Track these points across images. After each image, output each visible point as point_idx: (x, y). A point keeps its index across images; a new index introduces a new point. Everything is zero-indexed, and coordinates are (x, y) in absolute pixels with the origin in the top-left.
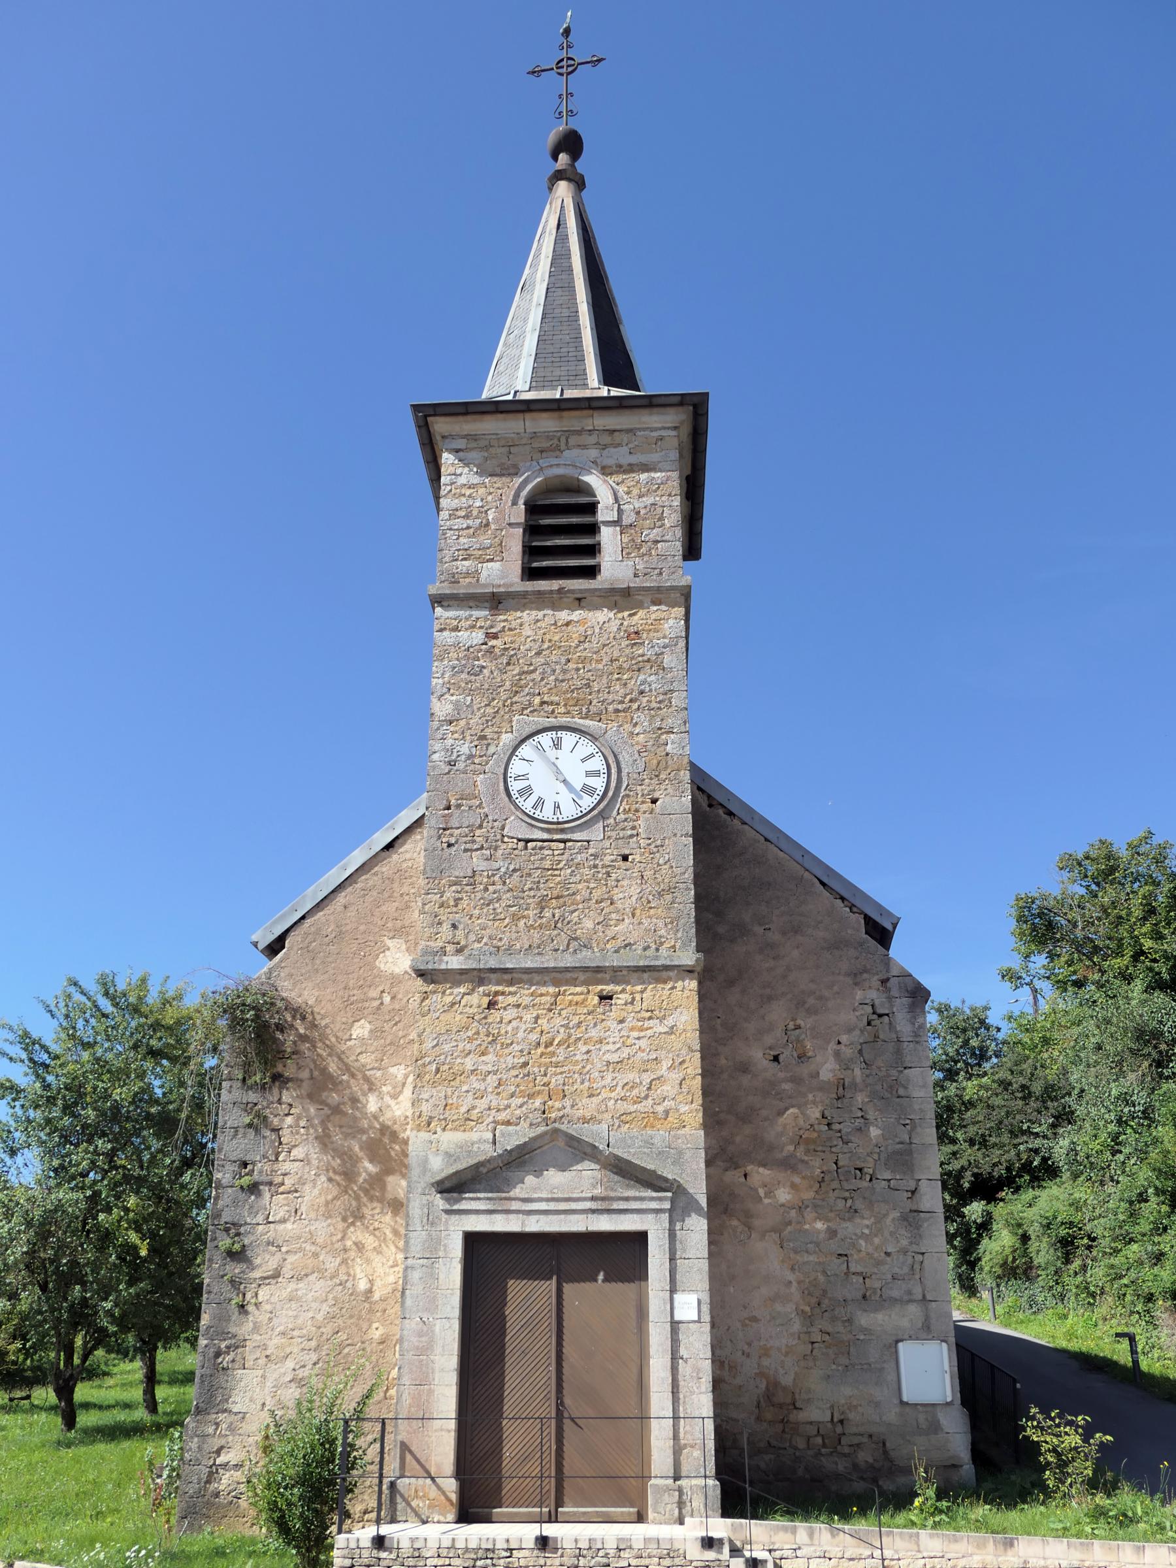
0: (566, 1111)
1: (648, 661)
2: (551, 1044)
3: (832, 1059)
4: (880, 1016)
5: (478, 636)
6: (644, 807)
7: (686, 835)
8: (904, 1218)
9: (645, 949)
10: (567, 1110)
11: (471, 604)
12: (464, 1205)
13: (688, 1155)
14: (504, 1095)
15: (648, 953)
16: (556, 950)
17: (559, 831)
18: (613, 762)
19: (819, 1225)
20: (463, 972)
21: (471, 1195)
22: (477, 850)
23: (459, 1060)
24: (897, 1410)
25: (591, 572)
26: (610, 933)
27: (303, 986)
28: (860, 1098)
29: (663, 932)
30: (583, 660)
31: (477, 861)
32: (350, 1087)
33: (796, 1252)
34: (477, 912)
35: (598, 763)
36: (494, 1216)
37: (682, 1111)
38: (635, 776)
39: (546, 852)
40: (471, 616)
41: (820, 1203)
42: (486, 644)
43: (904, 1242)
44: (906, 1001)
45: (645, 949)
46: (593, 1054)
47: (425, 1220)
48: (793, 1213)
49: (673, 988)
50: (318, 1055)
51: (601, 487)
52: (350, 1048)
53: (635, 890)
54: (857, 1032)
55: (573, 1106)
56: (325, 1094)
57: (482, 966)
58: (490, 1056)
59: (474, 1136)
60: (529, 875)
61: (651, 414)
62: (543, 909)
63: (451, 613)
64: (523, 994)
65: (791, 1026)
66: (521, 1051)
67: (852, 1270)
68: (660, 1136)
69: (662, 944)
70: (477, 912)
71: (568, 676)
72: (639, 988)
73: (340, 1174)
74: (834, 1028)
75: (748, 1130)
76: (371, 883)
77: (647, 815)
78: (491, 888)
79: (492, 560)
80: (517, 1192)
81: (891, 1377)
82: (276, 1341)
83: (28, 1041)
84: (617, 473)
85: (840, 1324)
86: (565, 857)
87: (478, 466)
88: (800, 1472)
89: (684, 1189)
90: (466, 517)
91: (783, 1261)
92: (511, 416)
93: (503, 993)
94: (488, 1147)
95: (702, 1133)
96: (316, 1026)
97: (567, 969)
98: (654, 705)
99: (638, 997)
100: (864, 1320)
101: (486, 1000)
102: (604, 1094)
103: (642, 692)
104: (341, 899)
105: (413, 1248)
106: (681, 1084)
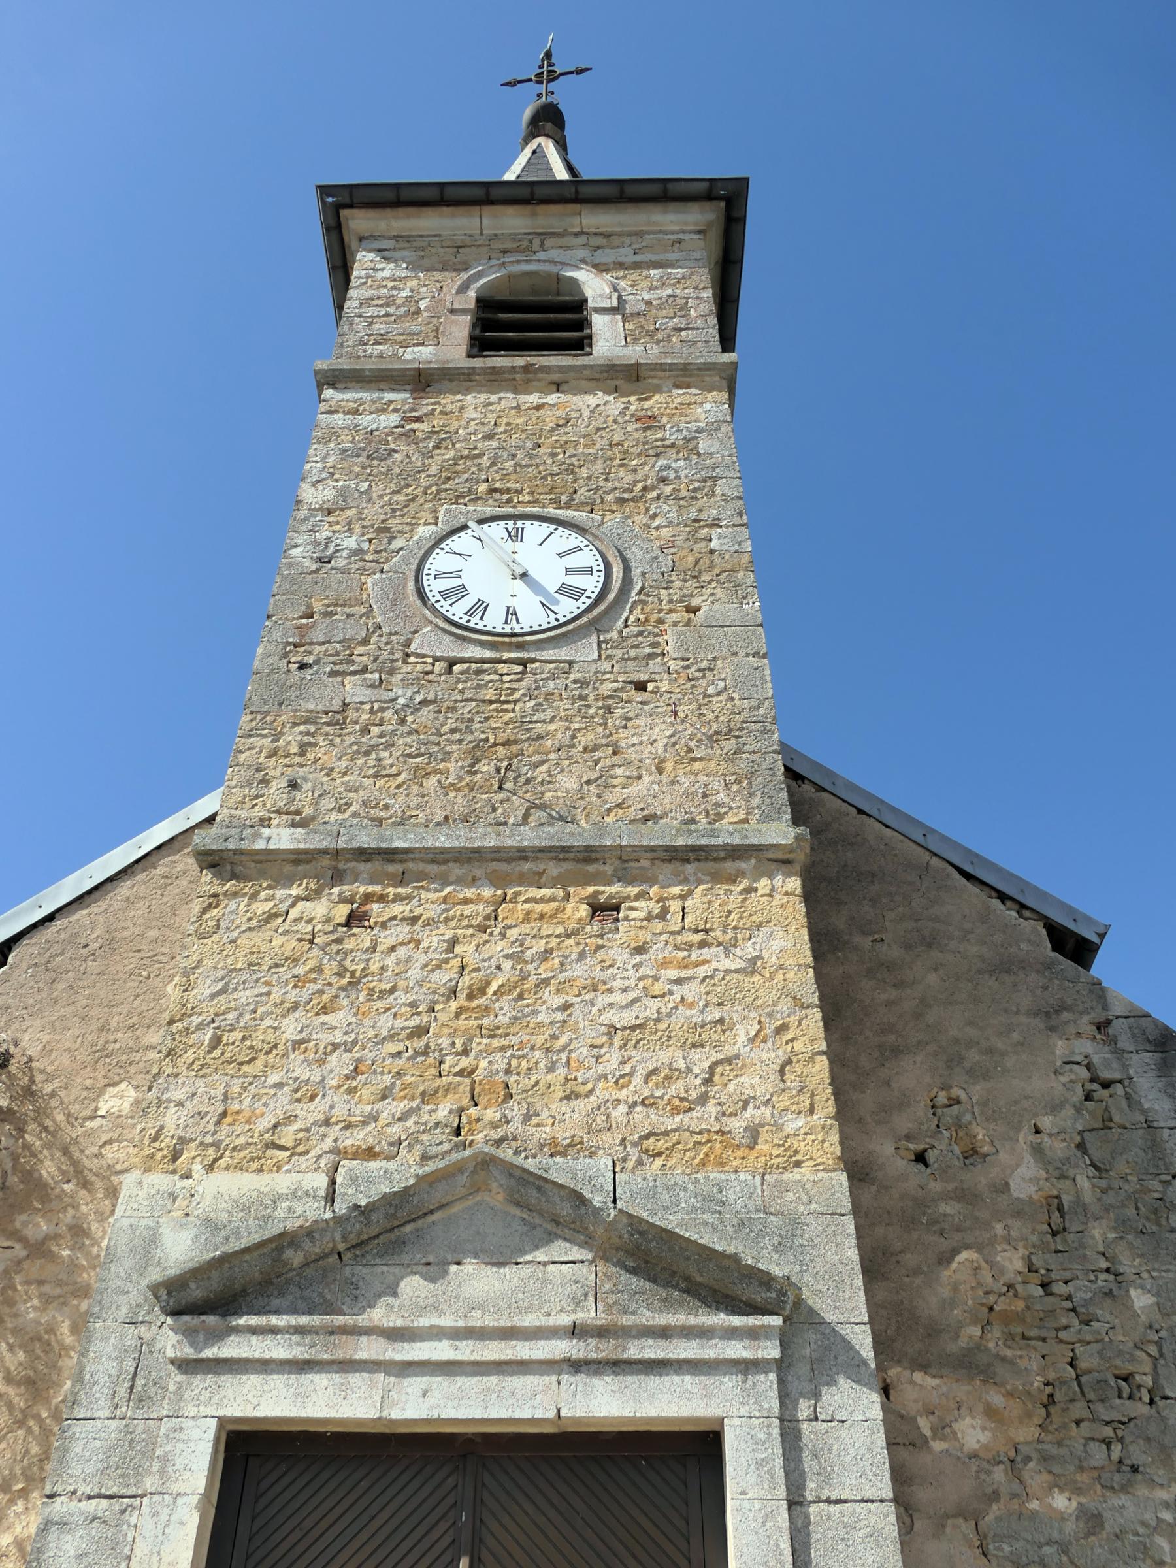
0: (511, 1128)
1: (673, 446)
2: (482, 991)
3: (1028, 1158)
4: (1106, 1085)
10: (515, 1126)
12: (232, 1348)
13: (814, 1227)
14: (366, 1093)
19: (1061, 1502)
20: (300, 858)
21: (254, 1320)
22: (355, 673)
23: (268, 1022)
25: (581, 344)
26: (613, 797)
27: (24, 1025)
28: (1098, 1233)
29: (722, 797)
31: (353, 689)
32: (76, 1207)
34: (343, 764)
36: (306, 1378)
37: (789, 1128)
40: (382, 398)
41: (1054, 1451)
46: (577, 1012)
47: (122, 1391)
48: (999, 1474)
49: (750, 890)
50: (26, 1146)
51: (595, 287)
52: (88, 1134)
53: (661, 733)
54: (1069, 1112)
55: (527, 1118)
56: (22, 1218)
57: (341, 845)
58: (341, 1015)
59: (283, 1182)
60: (454, 709)
61: (665, 212)
62: (476, 760)
63: (348, 395)
64: (428, 901)
65: (942, 1098)
66: (413, 1005)
68: (740, 1184)
69: (720, 816)
72: (676, 890)
73: (18, 1384)
74: (1026, 1104)
76: (180, 867)
77: (680, 628)
78: (375, 730)
79: (422, 344)
80: (378, 1315)
84: (615, 269)
86: (524, 684)
87: (408, 263)
89: (812, 1312)
92: (461, 210)
93: (382, 898)
95: (843, 1177)
96: (33, 1094)
97: (522, 854)
98: (684, 493)
99: (675, 906)
101: (343, 910)
103: (663, 480)
104: (124, 889)
106: (782, 1072)
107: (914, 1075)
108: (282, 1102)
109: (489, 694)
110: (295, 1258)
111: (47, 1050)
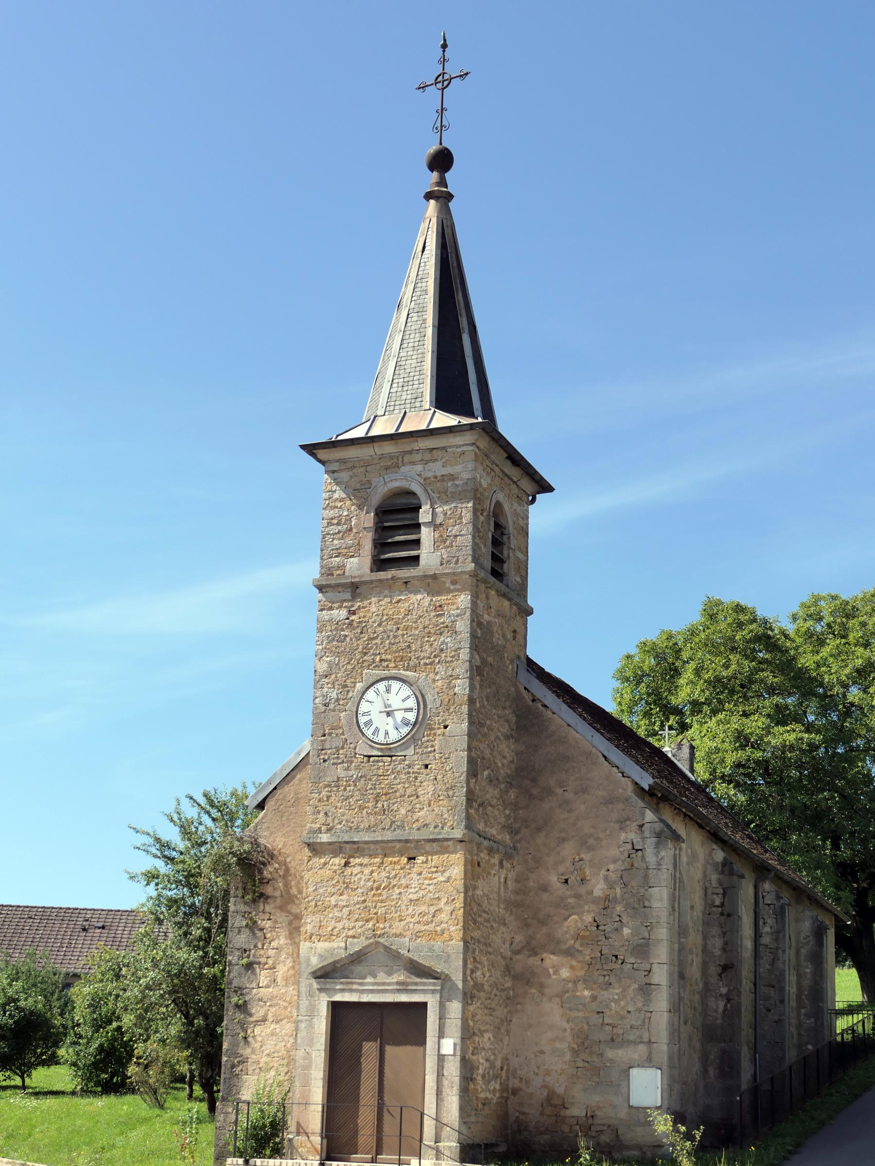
1: (447, 626)
3: (602, 881)
4: (637, 850)
5: (343, 613)
6: (439, 732)
7: (463, 751)
8: (641, 989)
9: (435, 827)
11: (340, 590)
13: (454, 956)
14: (352, 920)
15: (437, 830)
16: (384, 829)
17: (388, 751)
19: (586, 993)
22: (340, 763)
24: (627, 1110)
28: (619, 908)
29: (446, 816)
30: (406, 628)
31: (340, 771)
33: (571, 1010)
34: (339, 804)
35: (412, 703)
38: (434, 710)
39: (381, 764)
42: (348, 619)
43: (640, 1005)
44: (654, 840)
45: (435, 827)
48: (570, 985)
53: (431, 788)
54: (620, 863)
55: (390, 927)
56: (289, 906)
60: (370, 780)
62: (377, 802)
65: (577, 859)
67: (606, 1022)
70: (339, 804)
74: (605, 860)
75: (545, 930)
81: (624, 1090)
82: (264, 1059)
83: (164, 845)
85: (595, 1056)
88: (565, 1147)
90: (338, 524)
91: (562, 1016)
94: (343, 951)
95: (462, 943)
98: (449, 659)
100: (610, 1054)
101: (343, 861)
103: (442, 650)
105: (301, 1010)
108: (333, 923)
109: (380, 772)
110: (338, 965)
111: (285, 845)
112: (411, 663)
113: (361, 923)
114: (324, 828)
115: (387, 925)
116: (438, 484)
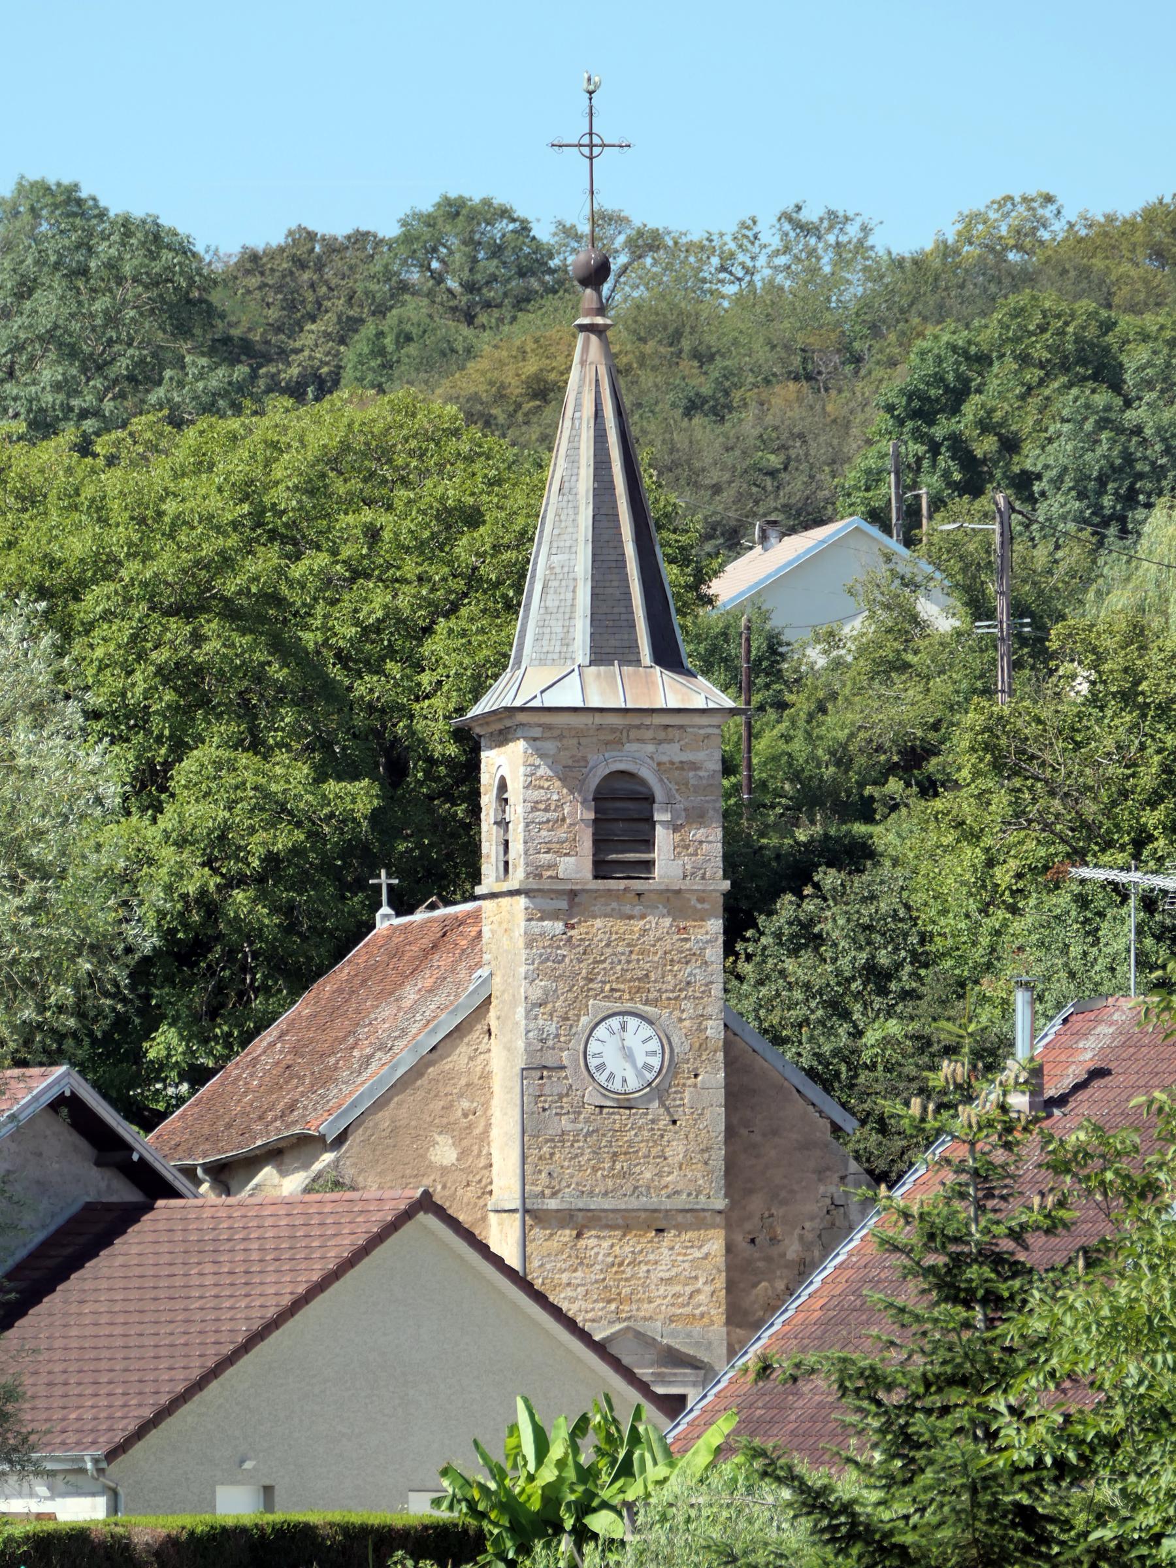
6: (689, 1082)
13: (716, 1344)
17: (626, 1104)
18: (666, 1041)
26: (663, 1183)
29: (700, 1182)
34: (566, 1164)
35: (654, 1045)
53: (681, 1149)
71: (631, 966)
79: (566, 855)
90: (546, 810)
101: (575, 1233)
102: (659, 1301)
103: (688, 983)
107: (756, 1204)
109: (617, 1126)
112: (651, 996)
113: (601, 1305)
114: (547, 1192)
115: (634, 1307)
116: (677, 773)
